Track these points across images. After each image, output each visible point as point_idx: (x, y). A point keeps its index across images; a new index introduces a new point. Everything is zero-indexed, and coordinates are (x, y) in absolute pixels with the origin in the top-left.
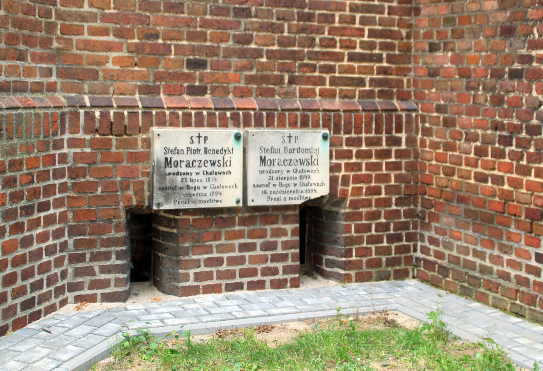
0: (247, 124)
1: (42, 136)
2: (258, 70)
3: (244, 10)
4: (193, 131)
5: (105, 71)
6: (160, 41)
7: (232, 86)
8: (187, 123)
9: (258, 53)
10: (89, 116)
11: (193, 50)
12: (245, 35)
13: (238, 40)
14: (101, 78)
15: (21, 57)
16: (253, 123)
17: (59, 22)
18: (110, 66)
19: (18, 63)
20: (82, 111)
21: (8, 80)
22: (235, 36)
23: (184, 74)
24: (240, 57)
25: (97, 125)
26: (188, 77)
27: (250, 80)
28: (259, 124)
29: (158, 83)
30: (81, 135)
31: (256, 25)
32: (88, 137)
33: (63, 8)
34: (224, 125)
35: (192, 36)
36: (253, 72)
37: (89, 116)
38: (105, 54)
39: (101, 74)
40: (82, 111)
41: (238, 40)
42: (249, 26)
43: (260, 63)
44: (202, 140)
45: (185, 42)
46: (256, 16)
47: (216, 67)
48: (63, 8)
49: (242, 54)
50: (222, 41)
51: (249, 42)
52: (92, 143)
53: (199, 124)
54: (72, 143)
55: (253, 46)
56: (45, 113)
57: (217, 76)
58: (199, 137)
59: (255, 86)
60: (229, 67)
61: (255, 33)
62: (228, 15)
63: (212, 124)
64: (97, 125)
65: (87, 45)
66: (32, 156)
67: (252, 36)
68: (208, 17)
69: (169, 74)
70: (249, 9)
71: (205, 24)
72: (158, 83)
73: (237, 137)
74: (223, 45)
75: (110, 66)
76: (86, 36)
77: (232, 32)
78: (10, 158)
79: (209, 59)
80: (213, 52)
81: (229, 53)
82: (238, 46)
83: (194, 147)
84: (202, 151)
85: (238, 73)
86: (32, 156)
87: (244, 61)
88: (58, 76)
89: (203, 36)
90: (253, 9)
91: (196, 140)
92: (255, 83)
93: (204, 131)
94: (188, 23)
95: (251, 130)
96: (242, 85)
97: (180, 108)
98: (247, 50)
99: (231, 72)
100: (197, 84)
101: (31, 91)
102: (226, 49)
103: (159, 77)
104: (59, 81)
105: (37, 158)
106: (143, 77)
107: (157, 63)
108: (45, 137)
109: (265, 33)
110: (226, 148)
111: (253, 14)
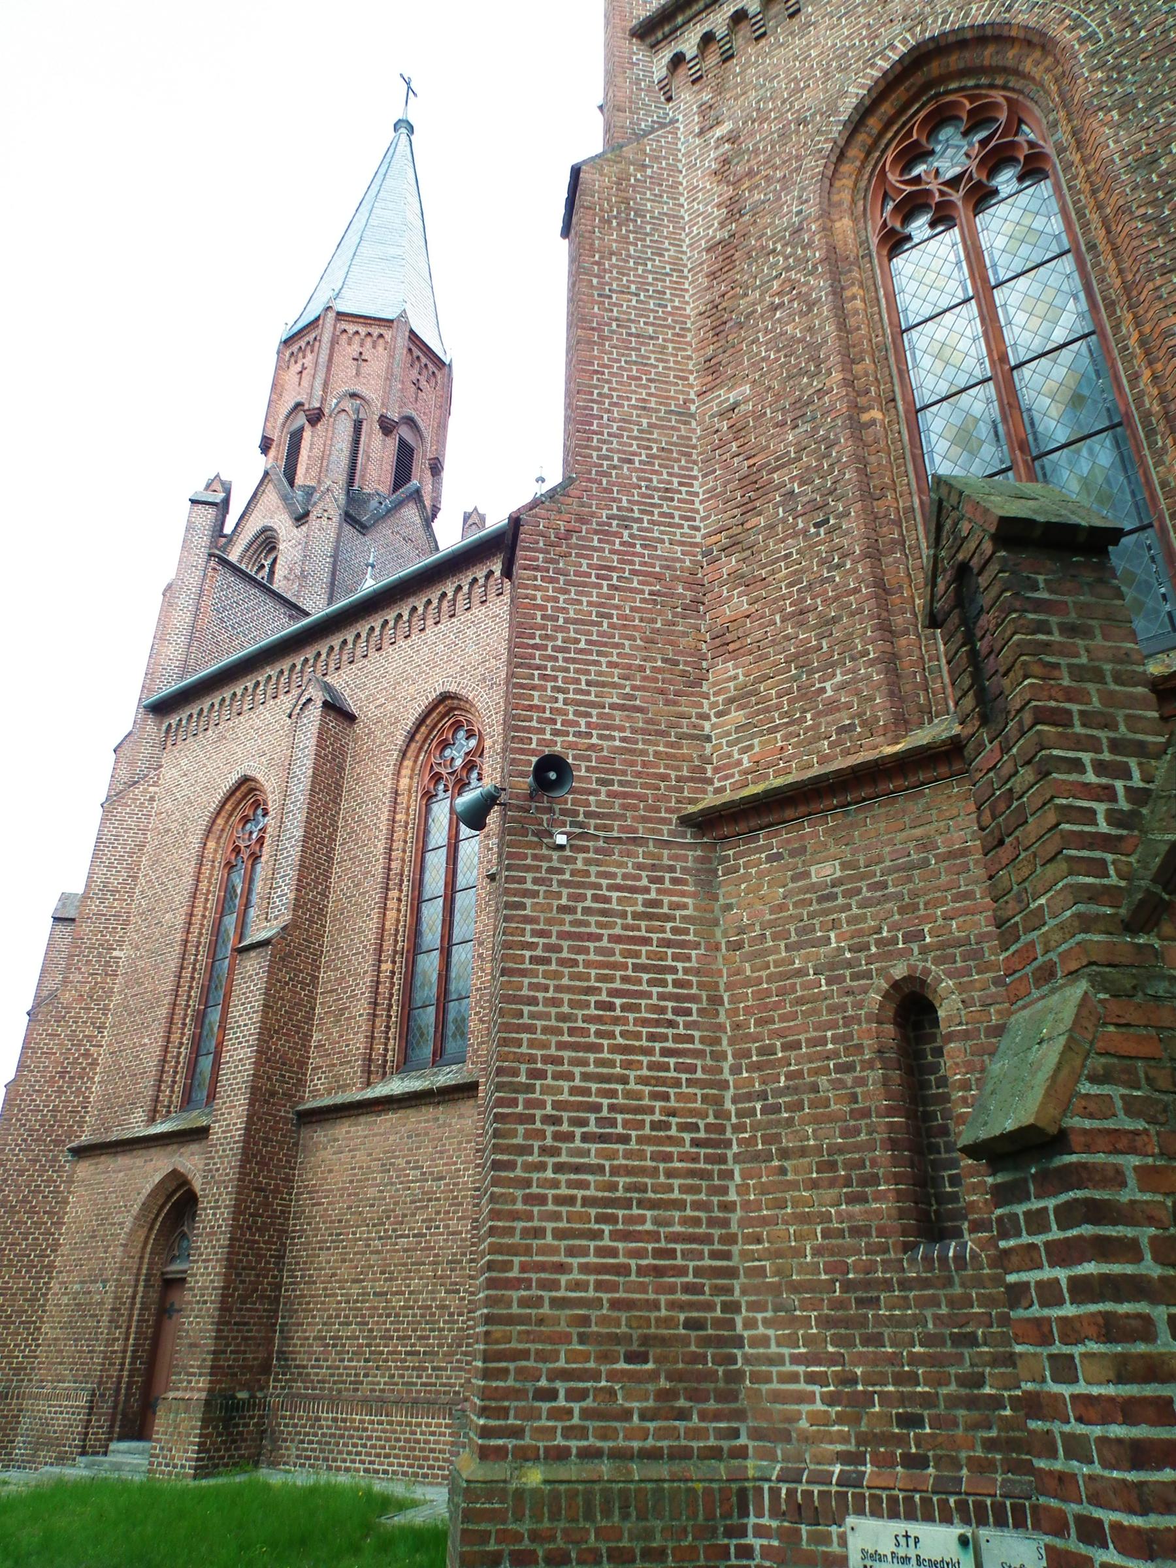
0: (982, 1522)
1: (701, 1518)
2: (999, 1430)
3: (965, 1335)
4: (899, 1527)
5: (798, 1430)
6: (860, 1388)
7: (963, 1455)
8: (894, 1515)
9: (997, 1402)
10: (775, 1492)
11: (903, 1399)
12: (972, 1374)
13: (962, 1381)
14: (794, 1441)
15: (683, 1415)
16: (991, 1520)
17: (747, 1368)
18: (803, 1424)
19: (677, 1423)
20: (766, 1486)
21: (659, 1444)
22: (957, 1376)
23: (894, 1435)
24: (968, 1409)
25: (784, 1507)
26: (901, 1440)
27: (990, 1445)
28: (1001, 1523)
29: (862, 1449)
30: (765, 1521)
31: (987, 1358)
32: (774, 1524)
33: (751, 1351)
34: (947, 1520)
35: (899, 1379)
36: (993, 1433)
37: (775, 1492)
38: (796, 1407)
39: (794, 1435)
40: (766, 1486)
41: (962, 1381)
42: (976, 1360)
43: (1001, 1418)
44: (911, 1541)
45: (891, 1388)
46: (985, 1344)
47: (936, 1423)
48: (751, 1351)
49: (972, 1403)
50: (940, 1385)
51: (980, 1384)
52: (781, 1533)
53: (910, 1516)
54: (760, 1531)
55: (987, 1390)
56: (705, 1489)
57: (940, 1439)
58: (907, 1536)
59: (999, 1457)
60: (955, 1424)
61: (988, 1370)
62: (944, 1344)
63: (928, 1518)
64: (784, 1507)
65: (777, 1397)
66: (684, 1544)
67: (983, 1375)
68: (917, 1349)
69: (875, 1435)
70: (973, 1335)
71: (914, 1360)
72: (862, 1449)
73: (963, 1541)
74: (944, 1391)
75: (803, 1424)
76: (775, 1385)
77: (952, 1370)
78: (642, 1544)
79: (926, 1413)
80: (928, 1401)
81: (953, 1402)
82: (964, 1391)
83: (901, 1552)
84: (914, 1561)
85: (971, 1433)
86: (684, 1544)
87: (976, 1415)
88: (749, 1437)
89: (913, 1379)
90: (980, 1332)
91: (902, 1541)
92: (999, 1451)
93: (916, 1528)
94: (893, 1359)
95: (983, 1532)
96: (979, 1453)
97: (884, 1489)
98: (978, 1397)
99: (960, 1432)
100: (914, 1450)
101: (546, 1458)
102: (948, 1397)
103: (862, 1439)
104: (751, 1444)
105: (693, 1549)
106: (844, 1439)
107: (857, 1420)
108: (706, 1519)
109: (1003, 1370)
110: (947, 1559)
111: (980, 1340)
